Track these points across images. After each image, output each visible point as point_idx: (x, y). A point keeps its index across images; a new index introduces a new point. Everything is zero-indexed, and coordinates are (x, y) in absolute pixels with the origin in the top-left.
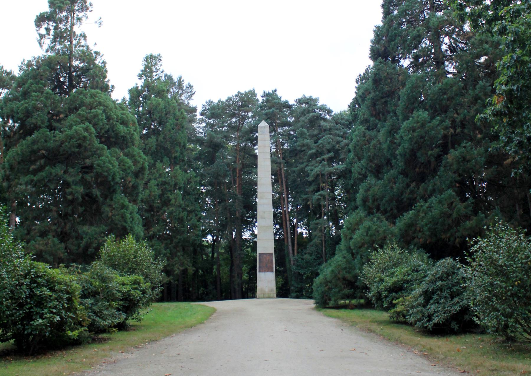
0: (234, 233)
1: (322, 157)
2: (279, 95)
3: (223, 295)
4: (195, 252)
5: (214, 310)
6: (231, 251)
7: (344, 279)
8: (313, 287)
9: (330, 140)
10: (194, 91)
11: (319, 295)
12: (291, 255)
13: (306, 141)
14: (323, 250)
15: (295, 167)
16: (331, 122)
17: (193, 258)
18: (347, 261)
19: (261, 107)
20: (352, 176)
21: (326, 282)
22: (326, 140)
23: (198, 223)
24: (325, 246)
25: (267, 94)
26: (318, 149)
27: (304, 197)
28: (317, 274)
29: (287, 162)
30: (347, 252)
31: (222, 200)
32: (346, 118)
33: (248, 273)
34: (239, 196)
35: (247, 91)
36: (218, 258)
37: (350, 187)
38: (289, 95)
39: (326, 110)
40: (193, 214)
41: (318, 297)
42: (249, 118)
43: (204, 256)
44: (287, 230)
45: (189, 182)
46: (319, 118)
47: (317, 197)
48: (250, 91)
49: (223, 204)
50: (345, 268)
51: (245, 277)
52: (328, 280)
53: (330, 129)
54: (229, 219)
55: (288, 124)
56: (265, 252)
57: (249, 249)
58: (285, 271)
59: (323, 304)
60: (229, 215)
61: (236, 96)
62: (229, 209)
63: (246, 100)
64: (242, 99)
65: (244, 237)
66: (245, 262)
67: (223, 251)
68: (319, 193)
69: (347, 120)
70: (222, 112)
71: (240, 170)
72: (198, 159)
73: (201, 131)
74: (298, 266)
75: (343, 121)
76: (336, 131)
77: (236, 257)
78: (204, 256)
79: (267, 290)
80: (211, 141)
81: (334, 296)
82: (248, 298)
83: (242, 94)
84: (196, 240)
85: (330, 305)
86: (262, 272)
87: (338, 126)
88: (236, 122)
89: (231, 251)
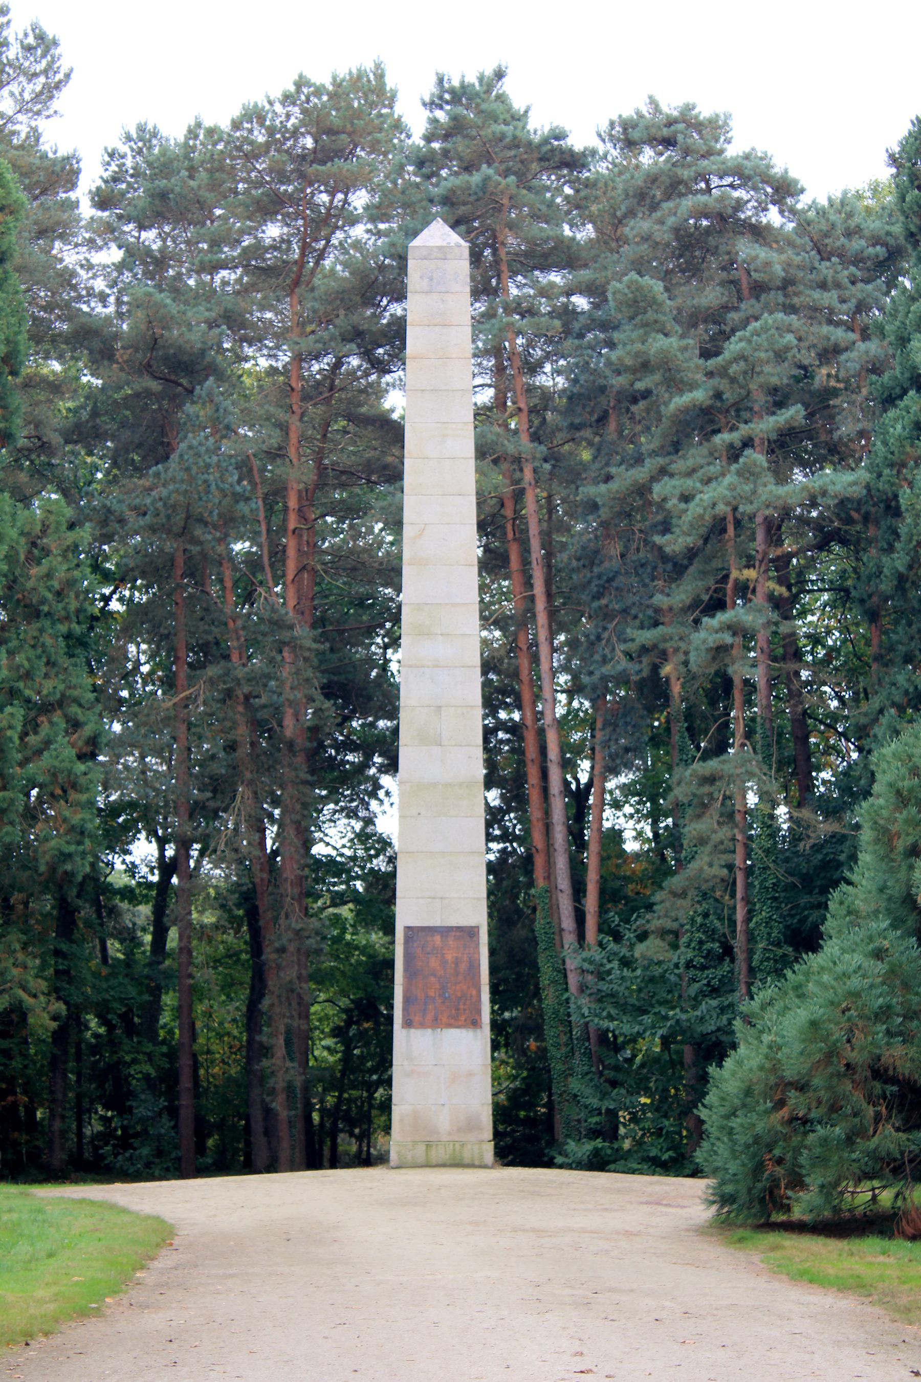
0: (271, 831)
1: (744, 430)
2: (518, 105)
3: (210, 1142)
4: (66, 919)
5: (163, 1234)
6: (253, 915)
7: (879, 1072)
8: (703, 1113)
9: (790, 338)
10: (64, 65)
11: (734, 1155)
12: (569, 939)
13: (658, 344)
14: (740, 916)
15: (596, 482)
16: (791, 244)
17: (57, 953)
18: (892, 972)
19: (420, 164)
20: (903, 530)
21: (780, 1088)
22: (765, 338)
23: (81, 767)
24: (747, 900)
25: (452, 91)
26: (722, 384)
27: (647, 636)
28: (716, 1048)
29: (552, 457)
30: (894, 926)
31: (210, 651)
32: (874, 225)
33: (337, 1032)
34: (298, 631)
35: (342, 73)
36: (185, 950)
37: (886, 586)
38: (573, 100)
39: (767, 179)
40: (57, 717)
41: (733, 1167)
42: (353, 221)
43: (115, 948)
44: (547, 813)
45: (36, 549)
46: (727, 220)
47: (713, 640)
48: (361, 74)
49: (212, 671)
50: (884, 1013)
51: (325, 1051)
52: (789, 1074)
53: (787, 284)
54: (245, 750)
55: (564, 256)
56: (438, 924)
57: (346, 911)
58: (534, 1027)
59: (759, 1207)
60: (243, 732)
61: (288, 99)
62: (247, 698)
63: (340, 126)
64: (315, 121)
65: (318, 850)
66: (321, 978)
67: (209, 918)
68: (721, 617)
69: (876, 241)
70: (214, 186)
71: (308, 497)
72: (84, 433)
73: (100, 285)
74: (601, 998)
75: (857, 244)
76: (817, 295)
77: (282, 950)
78: (115, 948)
79: (444, 1123)
80: (155, 343)
81: (820, 1161)
82: (335, 1163)
83: (318, 92)
84: (69, 856)
85: (798, 1213)
86: (422, 1025)
87: (826, 269)
88: (281, 245)
89: (253, 915)
